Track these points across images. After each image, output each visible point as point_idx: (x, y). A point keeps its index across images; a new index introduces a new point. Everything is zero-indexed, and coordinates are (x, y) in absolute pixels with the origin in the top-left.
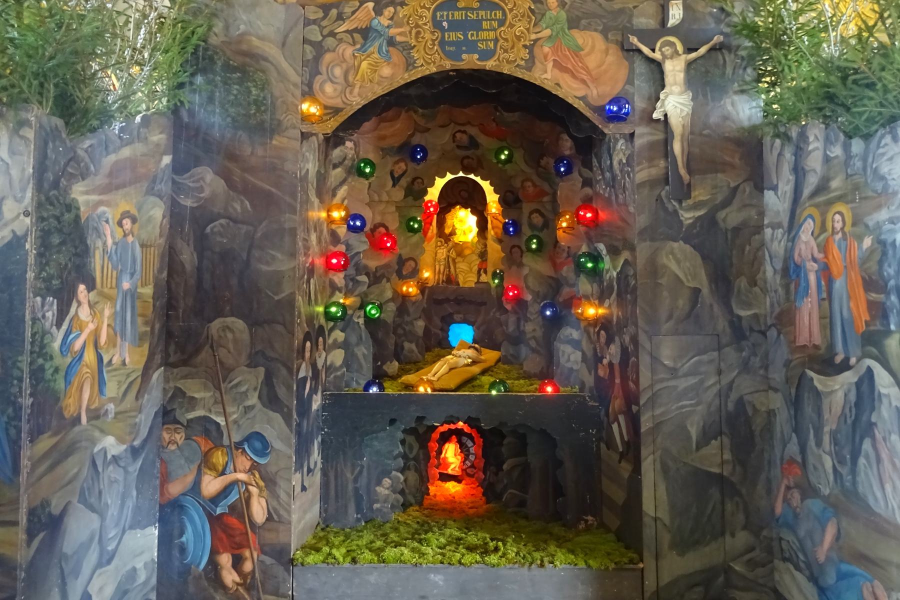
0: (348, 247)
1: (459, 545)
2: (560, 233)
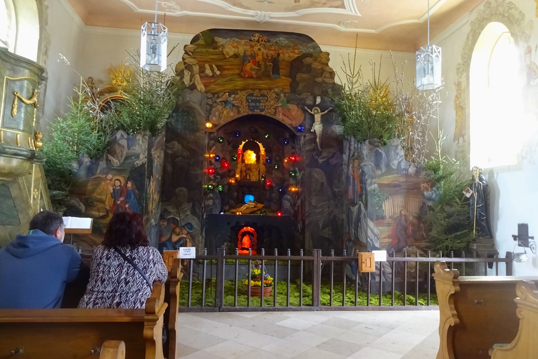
2: (284, 164)
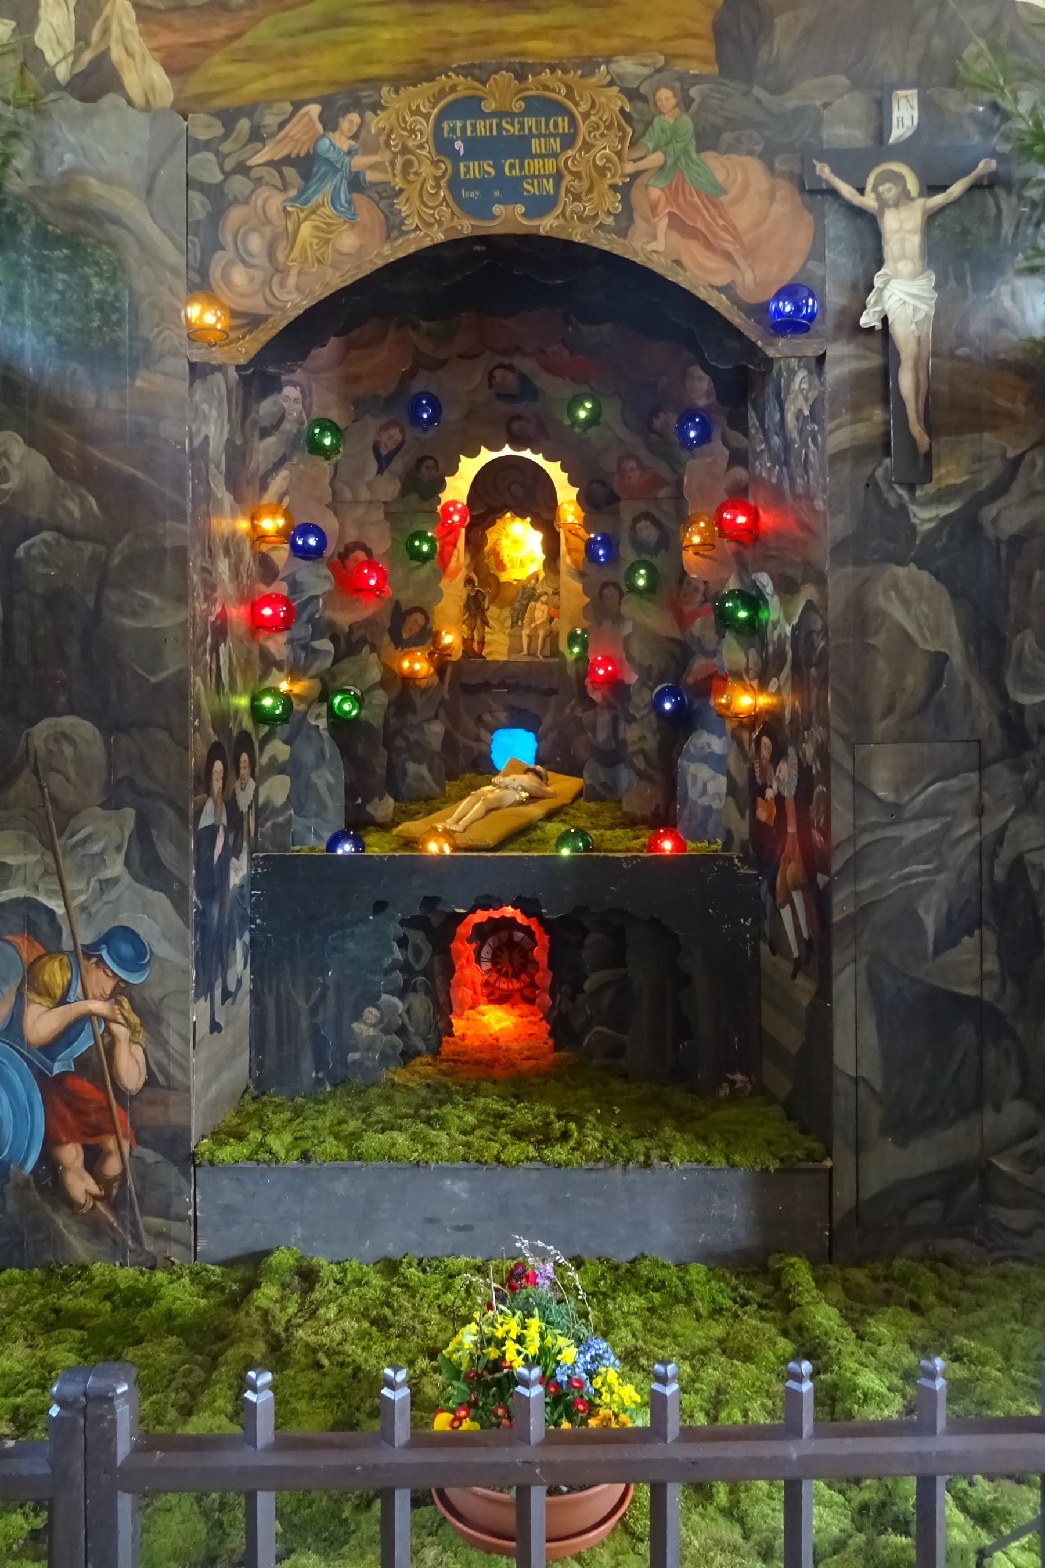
0: (295, 586)
1: (498, 1128)
2: (688, 556)
